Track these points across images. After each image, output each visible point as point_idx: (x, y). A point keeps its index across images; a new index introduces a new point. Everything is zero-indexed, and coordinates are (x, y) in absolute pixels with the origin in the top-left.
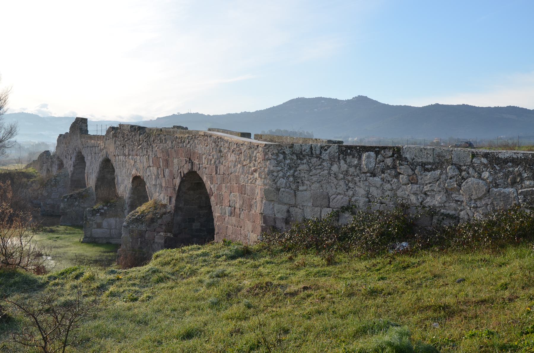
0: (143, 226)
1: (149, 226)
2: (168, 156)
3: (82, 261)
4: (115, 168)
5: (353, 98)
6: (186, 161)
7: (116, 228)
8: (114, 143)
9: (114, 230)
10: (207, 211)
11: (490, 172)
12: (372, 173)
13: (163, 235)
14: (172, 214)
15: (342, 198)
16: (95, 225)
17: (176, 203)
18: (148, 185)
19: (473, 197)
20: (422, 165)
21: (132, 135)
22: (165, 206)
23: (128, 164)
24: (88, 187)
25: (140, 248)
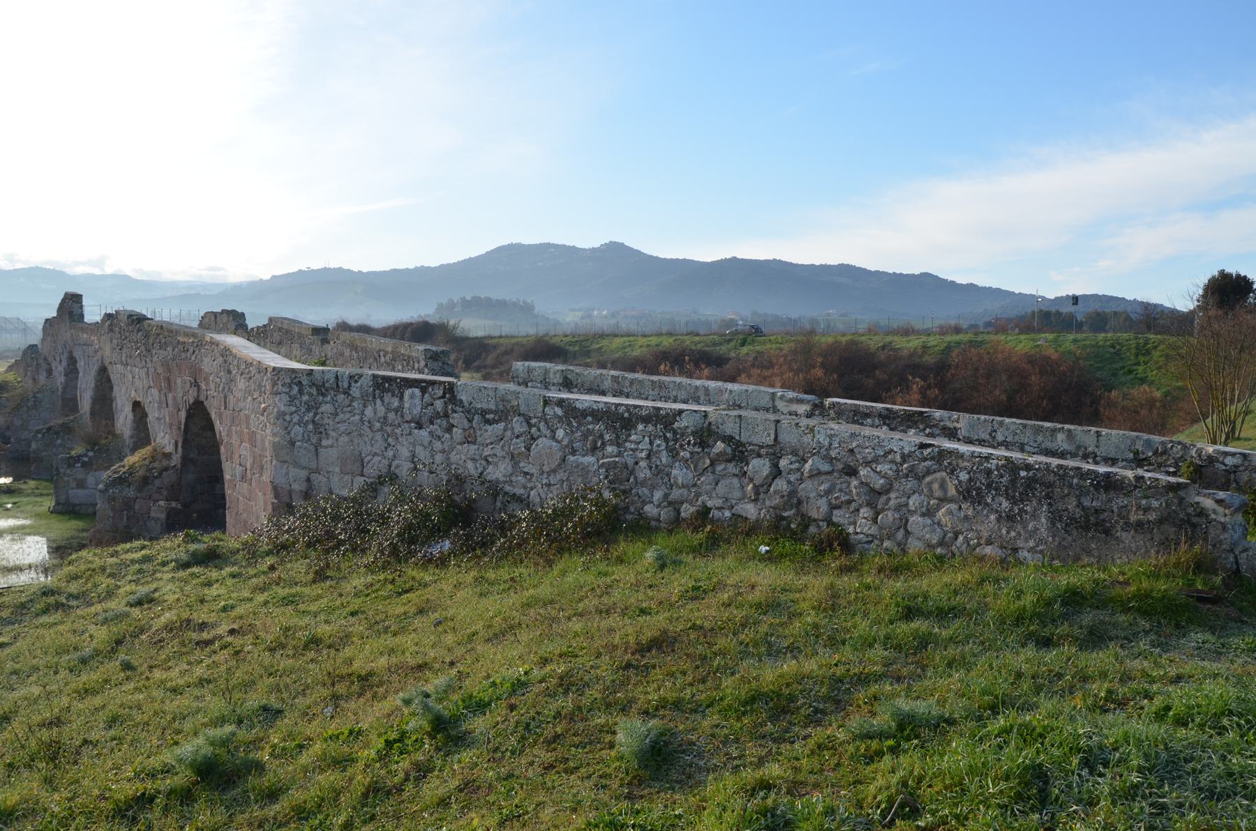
5: (602, 245)
6: (191, 384)
11: (565, 430)
12: (417, 423)
15: (380, 462)
17: (183, 452)
19: (546, 468)
20: (481, 414)
22: (168, 456)
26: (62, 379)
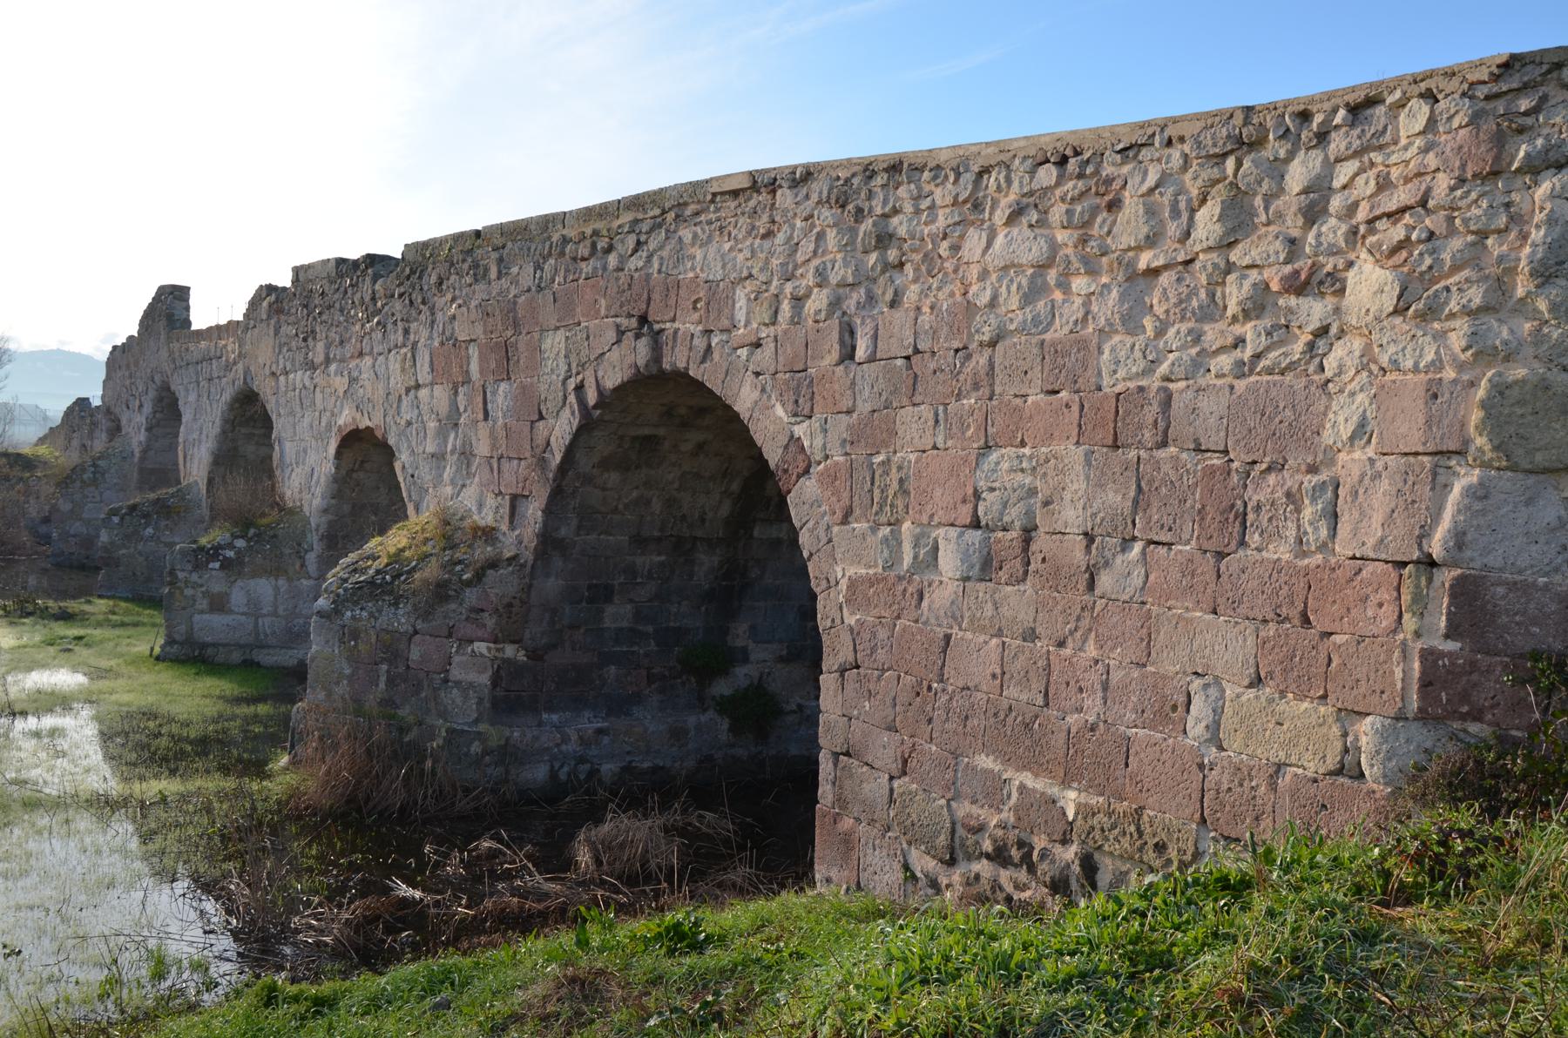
0: (401, 612)
1: (426, 615)
2: (516, 324)
3: (149, 745)
4: (274, 418)
6: (621, 333)
7: (275, 614)
8: (272, 332)
9: (267, 621)
10: (663, 558)
13: (485, 652)
14: (523, 566)
16: (205, 602)
18: (403, 458)
21: (342, 289)
22: (488, 534)
23: (322, 392)
24: (184, 483)
25: (387, 702)
26: (142, 436)
